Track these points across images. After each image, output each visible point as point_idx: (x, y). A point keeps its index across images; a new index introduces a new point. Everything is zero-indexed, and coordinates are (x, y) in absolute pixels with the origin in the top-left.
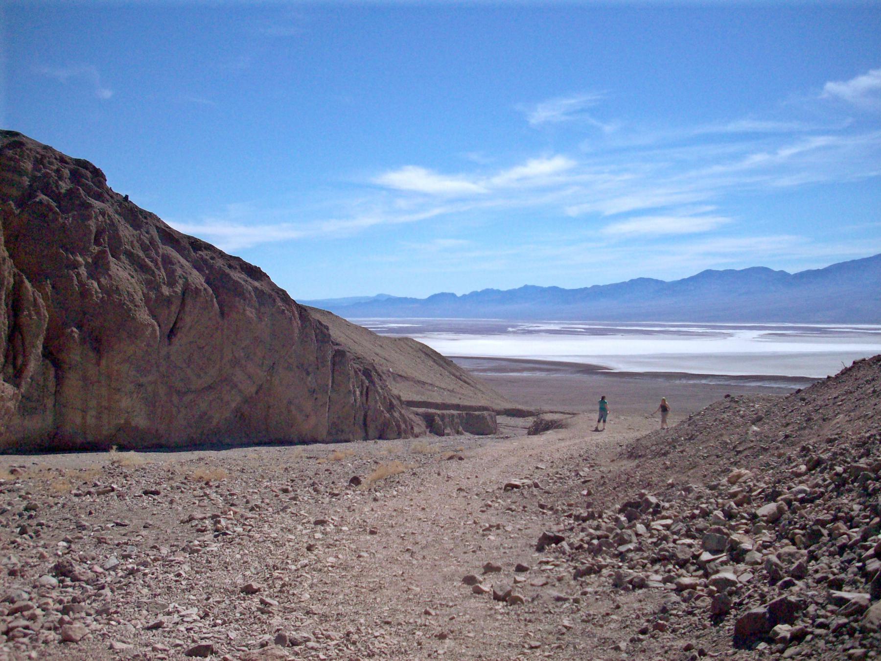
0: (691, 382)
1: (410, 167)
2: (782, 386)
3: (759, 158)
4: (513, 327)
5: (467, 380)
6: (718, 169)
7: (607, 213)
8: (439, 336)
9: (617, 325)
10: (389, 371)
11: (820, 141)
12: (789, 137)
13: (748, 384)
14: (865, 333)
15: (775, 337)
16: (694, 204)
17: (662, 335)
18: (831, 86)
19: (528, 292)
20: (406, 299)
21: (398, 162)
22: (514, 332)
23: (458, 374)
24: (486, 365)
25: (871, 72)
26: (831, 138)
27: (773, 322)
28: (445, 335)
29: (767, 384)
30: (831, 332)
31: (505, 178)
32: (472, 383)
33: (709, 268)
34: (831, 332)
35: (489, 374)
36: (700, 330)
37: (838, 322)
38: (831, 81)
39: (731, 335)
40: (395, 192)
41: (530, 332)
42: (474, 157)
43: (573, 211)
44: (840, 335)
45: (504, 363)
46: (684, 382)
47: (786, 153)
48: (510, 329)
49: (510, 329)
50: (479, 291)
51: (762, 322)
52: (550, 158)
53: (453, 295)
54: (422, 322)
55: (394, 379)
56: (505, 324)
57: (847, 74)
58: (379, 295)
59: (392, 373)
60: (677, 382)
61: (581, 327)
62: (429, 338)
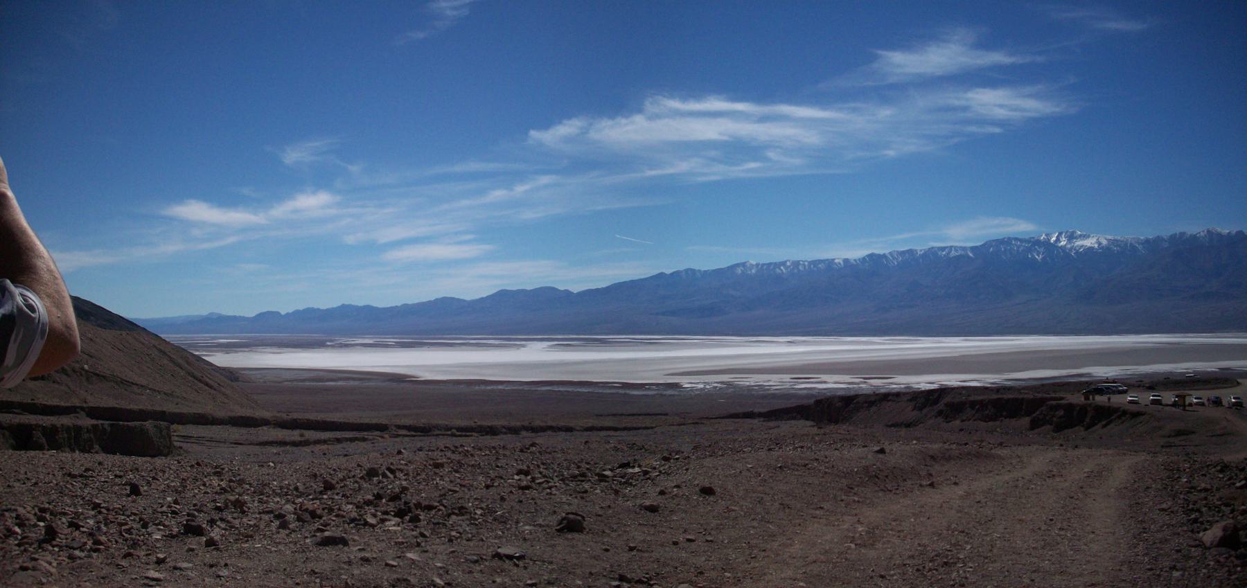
0: (489, 388)
1: (193, 201)
2: (570, 389)
3: (498, 194)
4: (331, 341)
5: (210, 382)
6: (465, 203)
7: (383, 241)
8: (265, 350)
9: (421, 339)
10: (83, 369)
11: (545, 180)
12: (520, 177)
13: (539, 389)
14: (677, 344)
15: (562, 347)
16: (456, 233)
17: (464, 347)
18: (534, 134)
19: (346, 311)
20: (135, 324)
21: (181, 196)
22: (332, 346)
23: (198, 374)
24: (307, 375)
25: (565, 122)
26: (554, 177)
27: (560, 334)
28: (269, 349)
29: (556, 388)
30: (610, 342)
31: (280, 211)
32: (216, 385)
33: (503, 288)
34: (610, 342)
35: (307, 383)
36: (497, 342)
37: (613, 334)
38: (533, 129)
39: (523, 346)
40: (186, 224)
41: (346, 346)
42: (246, 191)
43: (350, 240)
44: (623, 344)
45: (321, 373)
46: (483, 387)
47: (520, 189)
48: (328, 343)
49: (328, 343)
50: (301, 309)
51: (551, 334)
52: (314, 193)
53: (278, 313)
54: (248, 338)
55: (88, 379)
56: (324, 338)
57: (546, 125)
58: (210, 314)
59: (87, 371)
60: (477, 388)
61: (391, 341)
62: (253, 352)
